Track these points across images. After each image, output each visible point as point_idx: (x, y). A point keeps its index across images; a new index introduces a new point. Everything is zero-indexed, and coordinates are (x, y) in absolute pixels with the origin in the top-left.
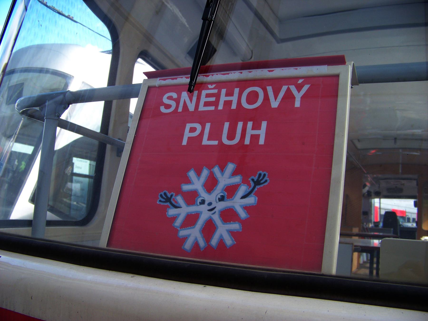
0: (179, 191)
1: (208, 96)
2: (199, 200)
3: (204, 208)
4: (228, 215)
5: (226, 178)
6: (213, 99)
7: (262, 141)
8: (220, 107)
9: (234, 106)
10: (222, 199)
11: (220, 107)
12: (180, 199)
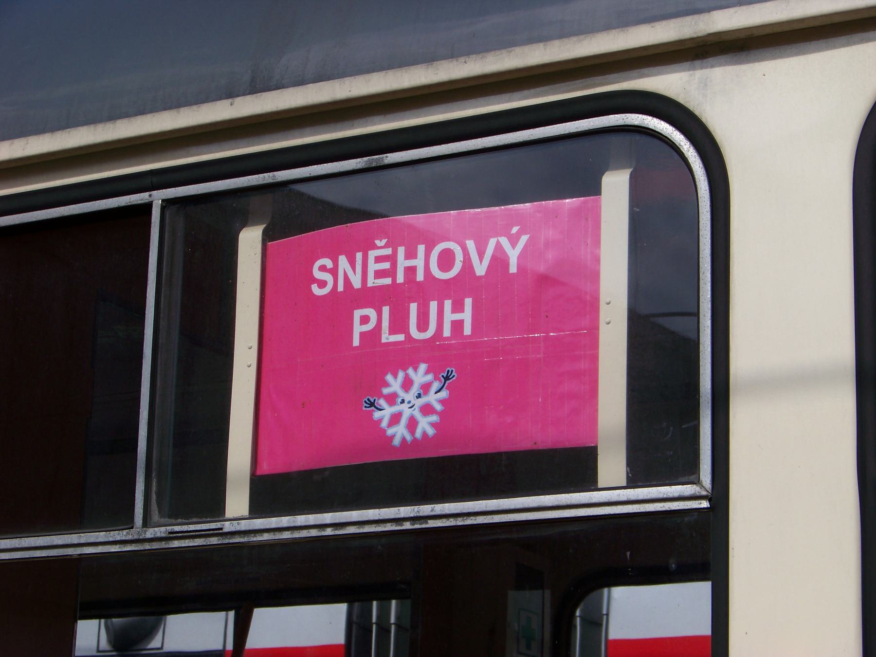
0: (381, 395)
1: (378, 259)
2: (399, 400)
3: (405, 407)
4: (427, 410)
5: (420, 375)
6: (386, 265)
7: (467, 330)
8: (400, 279)
9: (420, 277)
10: (419, 396)
11: (400, 279)
12: (382, 402)
